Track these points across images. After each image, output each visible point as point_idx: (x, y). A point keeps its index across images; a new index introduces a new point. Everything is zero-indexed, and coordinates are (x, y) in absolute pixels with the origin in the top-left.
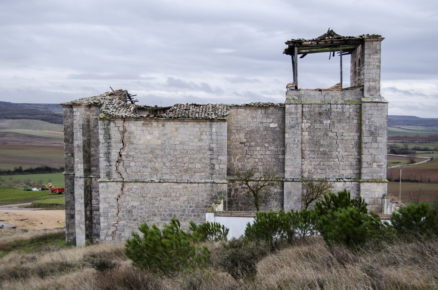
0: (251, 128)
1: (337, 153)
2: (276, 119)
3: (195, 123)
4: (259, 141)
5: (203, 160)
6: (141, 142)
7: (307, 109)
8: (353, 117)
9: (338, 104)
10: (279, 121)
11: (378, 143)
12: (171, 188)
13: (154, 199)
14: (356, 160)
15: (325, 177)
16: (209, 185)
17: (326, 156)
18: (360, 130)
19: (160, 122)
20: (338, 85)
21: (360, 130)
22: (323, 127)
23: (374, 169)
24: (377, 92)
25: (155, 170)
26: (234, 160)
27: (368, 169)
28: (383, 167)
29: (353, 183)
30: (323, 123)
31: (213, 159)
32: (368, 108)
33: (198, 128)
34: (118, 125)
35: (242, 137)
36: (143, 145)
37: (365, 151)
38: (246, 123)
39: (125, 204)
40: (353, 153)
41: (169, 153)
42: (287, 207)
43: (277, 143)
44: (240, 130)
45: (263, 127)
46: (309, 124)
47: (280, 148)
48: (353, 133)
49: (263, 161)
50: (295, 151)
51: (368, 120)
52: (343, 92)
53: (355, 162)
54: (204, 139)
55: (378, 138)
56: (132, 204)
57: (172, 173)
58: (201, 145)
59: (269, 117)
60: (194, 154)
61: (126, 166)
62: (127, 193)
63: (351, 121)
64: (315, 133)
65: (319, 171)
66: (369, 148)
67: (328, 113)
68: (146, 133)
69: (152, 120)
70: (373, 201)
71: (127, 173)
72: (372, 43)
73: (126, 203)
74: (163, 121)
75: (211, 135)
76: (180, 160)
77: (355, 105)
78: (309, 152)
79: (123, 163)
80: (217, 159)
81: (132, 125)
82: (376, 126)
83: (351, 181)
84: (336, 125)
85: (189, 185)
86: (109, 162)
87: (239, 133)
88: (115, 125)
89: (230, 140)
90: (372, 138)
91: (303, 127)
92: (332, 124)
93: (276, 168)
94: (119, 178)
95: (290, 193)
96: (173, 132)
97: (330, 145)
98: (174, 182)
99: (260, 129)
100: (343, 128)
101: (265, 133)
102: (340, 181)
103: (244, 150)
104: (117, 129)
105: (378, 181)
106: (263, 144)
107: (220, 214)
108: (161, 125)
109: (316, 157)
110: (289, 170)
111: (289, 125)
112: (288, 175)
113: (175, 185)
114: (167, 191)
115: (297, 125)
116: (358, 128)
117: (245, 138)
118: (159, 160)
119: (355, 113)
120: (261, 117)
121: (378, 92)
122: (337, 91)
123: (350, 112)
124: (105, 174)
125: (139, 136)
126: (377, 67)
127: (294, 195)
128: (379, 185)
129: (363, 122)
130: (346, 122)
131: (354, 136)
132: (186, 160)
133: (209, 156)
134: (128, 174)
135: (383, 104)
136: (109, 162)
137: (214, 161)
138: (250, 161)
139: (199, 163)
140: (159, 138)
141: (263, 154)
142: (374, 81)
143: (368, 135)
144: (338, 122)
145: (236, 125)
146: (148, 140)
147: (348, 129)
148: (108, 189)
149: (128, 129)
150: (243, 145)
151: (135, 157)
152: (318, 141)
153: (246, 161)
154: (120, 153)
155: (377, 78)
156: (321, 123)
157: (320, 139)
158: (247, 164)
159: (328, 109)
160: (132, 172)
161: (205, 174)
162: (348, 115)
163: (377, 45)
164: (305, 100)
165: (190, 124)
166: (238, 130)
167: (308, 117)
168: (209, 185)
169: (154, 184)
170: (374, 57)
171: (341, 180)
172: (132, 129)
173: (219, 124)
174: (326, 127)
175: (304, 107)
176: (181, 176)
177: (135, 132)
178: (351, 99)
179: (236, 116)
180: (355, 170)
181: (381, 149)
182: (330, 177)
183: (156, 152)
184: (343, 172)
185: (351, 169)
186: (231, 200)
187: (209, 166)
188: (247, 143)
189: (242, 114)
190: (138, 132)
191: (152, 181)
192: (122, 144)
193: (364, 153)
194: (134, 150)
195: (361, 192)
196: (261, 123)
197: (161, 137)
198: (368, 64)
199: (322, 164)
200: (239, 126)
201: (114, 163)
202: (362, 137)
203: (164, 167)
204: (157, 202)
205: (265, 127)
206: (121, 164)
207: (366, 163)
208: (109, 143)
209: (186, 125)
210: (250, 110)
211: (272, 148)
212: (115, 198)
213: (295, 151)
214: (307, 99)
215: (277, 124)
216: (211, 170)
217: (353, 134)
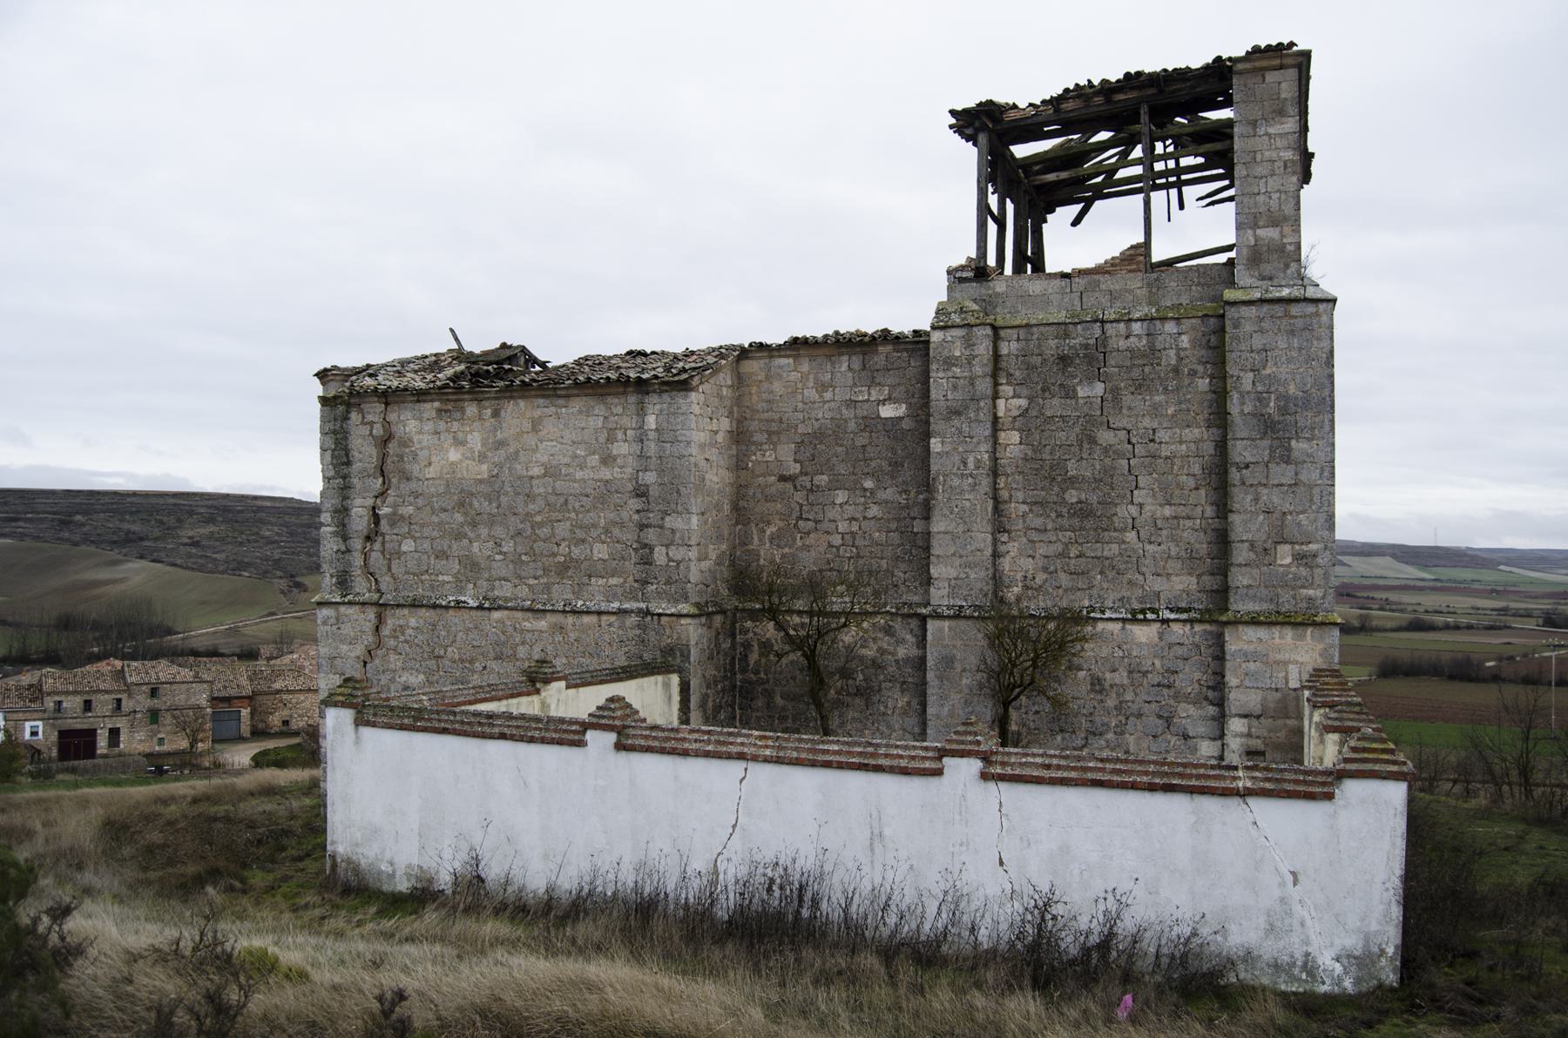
0: (817, 425)
1: (1133, 510)
2: (902, 388)
3: (591, 401)
4: (842, 469)
5: (616, 531)
6: (431, 472)
7: (1014, 345)
8: (1194, 367)
9: (1130, 320)
10: (913, 396)
11: (1297, 464)
12: (515, 629)
13: (467, 665)
14: (1211, 536)
15: (1087, 603)
16: (633, 620)
17: (1089, 524)
18: (1220, 417)
19: (486, 403)
20: (1132, 252)
21: (1220, 417)
22: (1076, 410)
23: (1282, 569)
24: (1287, 266)
25: (472, 567)
26: (760, 540)
27: (1256, 572)
28: (1319, 560)
29: (1198, 628)
30: (1075, 397)
31: (648, 526)
32: (1248, 327)
33: (601, 418)
34: (370, 418)
35: (785, 456)
36: (437, 482)
37: (1241, 499)
38: (800, 405)
39: (384, 680)
40: (1199, 509)
41: (510, 507)
42: (938, 716)
43: (907, 473)
44: (778, 433)
45: (856, 417)
46: (1023, 402)
47: (918, 493)
48: (1196, 430)
49: (857, 543)
50: (968, 504)
51: (1251, 374)
52: (1154, 275)
53: (1205, 546)
54: (619, 455)
55: (1293, 443)
56: (404, 679)
57: (520, 577)
58: (609, 477)
59: (877, 381)
60: (588, 511)
61: (391, 554)
62: (392, 643)
63: (1187, 381)
64: (1047, 434)
65: (1064, 579)
66: (1260, 484)
67: (1095, 359)
68: (447, 439)
69: (462, 397)
70: (1279, 701)
71: (393, 576)
72: (1259, 79)
73: (388, 676)
74: (495, 398)
75: (642, 441)
76: (544, 532)
77: (1199, 321)
78: (1025, 508)
79: (383, 543)
80: (661, 527)
81: (409, 415)
82: (1281, 397)
83: (1191, 621)
84: (1127, 399)
85: (570, 619)
86: (345, 538)
87: (775, 444)
88: (363, 418)
89: (746, 468)
90: (1271, 446)
91: (1000, 414)
92: (1109, 397)
93: (903, 566)
94: (370, 591)
95: (948, 661)
96: (525, 436)
97: (1104, 479)
98: (523, 610)
99: (846, 427)
100: (1155, 410)
101: (861, 441)
102: (1145, 620)
103: (794, 505)
104: (365, 430)
105: (1299, 620)
106: (856, 482)
107: (375, 715)
108: (489, 411)
109: (1050, 526)
110: (945, 576)
111: (942, 404)
112: (941, 593)
113: (527, 620)
114: (503, 638)
115: (972, 406)
116: (1212, 410)
117: (796, 461)
118: (484, 531)
119: (1203, 352)
120: (850, 382)
121: (1294, 265)
122: (1131, 275)
123: (1179, 349)
124: (334, 580)
125: (425, 453)
126: (1285, 167)
127: (964, 670)
128: (1302, 637)
129: (1229, 381)
130: (1166, 389)
131: (1201, 440)
132: (562, 529)
133: (636, 517)
134: (394, 579)
135: (1310, 309)
136: (345, 541)
137: (651, 536)
138: (813, 542)
139: (603, 543)
140: (482, 458)
141: (858, 515)
142: (1274, 223)
143: (1254, 434)
144: (1132, 389)
145: (766, 415)
146: (452, 463)
147: (1173, 416)
148: (339, 628)
149: (398, 430)
150: (789, 486)
151: (416, 524)
152: (1059, 465)
153: (799, 543)
154: (374, 508)
155: (1288, 209)
156: (1070, 394)
157: (1067, 457)
158: (803, 555)
159: (1092, 341)
160: (407, 573)
161: (621, 580)
162: (1173, 362)
163: (1283, 85)
164: (1008, 316)
165: (577, 404)
166: (773, 433)
167: (1017, 373)
168: (633, 620)
169: (466, 615)
170: (1271, 130)
171: (1150, 616)
172: (407, 429)
173: (669, 400)
174: (1086, 409)
175: (1003, 339)
176: (547, 588)
177: (416, 438)
178: (1184, 300)
179: (765, 385)
180: (1205, 578)
181: (1311, 487)
182: (1106, 604)
183: (476, 504)
184: (1157, 584)
185: (1190, 574)
186: (750, 683)
187: (633, 554)
188: (804, 478)
189: (785, 375)
190: (426, 439)
191: (459, 605)
192: (381, 480)
193: (1236, 506)
194: (412, 499)
195: (1228, 665)
196: (851, 403)
197: (489, 454)
198: (1248, 159)
199: (1073, 552)
200: (776, 416)
201: (357, 544)
202: (1230, 443)
203: (498, 557)
204: (476, 677)
205: (864, 418)
206: (377, 546)
207: (1247, 544)
208: (344, 477)
209: (564, 410)
210: (812, 358)
211: (889, 494)
212: (358, 658)
213: (968, 504)
214: (1018, 312)
215: (904, 406)
216: (642, 567)
217: (1196, 433)
